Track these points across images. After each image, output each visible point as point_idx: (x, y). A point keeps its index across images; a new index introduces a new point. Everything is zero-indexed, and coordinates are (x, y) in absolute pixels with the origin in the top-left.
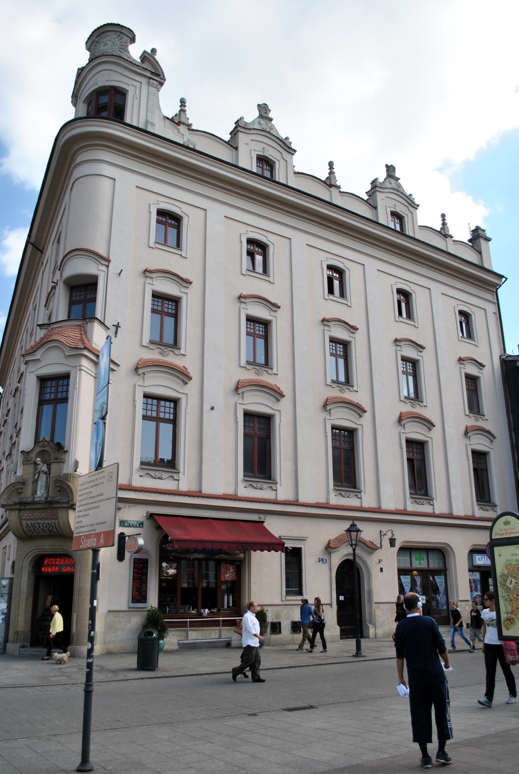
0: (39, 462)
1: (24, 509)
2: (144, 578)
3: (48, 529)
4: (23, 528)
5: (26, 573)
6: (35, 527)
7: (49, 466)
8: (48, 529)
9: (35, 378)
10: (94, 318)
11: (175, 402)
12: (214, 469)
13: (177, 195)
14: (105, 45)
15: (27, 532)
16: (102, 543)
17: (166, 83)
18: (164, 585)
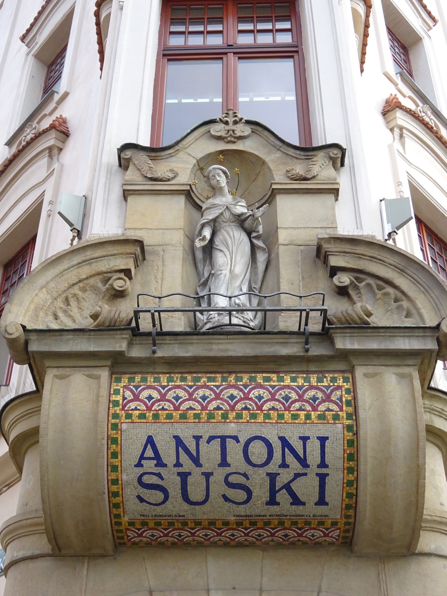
3: (273, 477)
6: (196, 461)
8: (273, 477)
15: (130, 492)
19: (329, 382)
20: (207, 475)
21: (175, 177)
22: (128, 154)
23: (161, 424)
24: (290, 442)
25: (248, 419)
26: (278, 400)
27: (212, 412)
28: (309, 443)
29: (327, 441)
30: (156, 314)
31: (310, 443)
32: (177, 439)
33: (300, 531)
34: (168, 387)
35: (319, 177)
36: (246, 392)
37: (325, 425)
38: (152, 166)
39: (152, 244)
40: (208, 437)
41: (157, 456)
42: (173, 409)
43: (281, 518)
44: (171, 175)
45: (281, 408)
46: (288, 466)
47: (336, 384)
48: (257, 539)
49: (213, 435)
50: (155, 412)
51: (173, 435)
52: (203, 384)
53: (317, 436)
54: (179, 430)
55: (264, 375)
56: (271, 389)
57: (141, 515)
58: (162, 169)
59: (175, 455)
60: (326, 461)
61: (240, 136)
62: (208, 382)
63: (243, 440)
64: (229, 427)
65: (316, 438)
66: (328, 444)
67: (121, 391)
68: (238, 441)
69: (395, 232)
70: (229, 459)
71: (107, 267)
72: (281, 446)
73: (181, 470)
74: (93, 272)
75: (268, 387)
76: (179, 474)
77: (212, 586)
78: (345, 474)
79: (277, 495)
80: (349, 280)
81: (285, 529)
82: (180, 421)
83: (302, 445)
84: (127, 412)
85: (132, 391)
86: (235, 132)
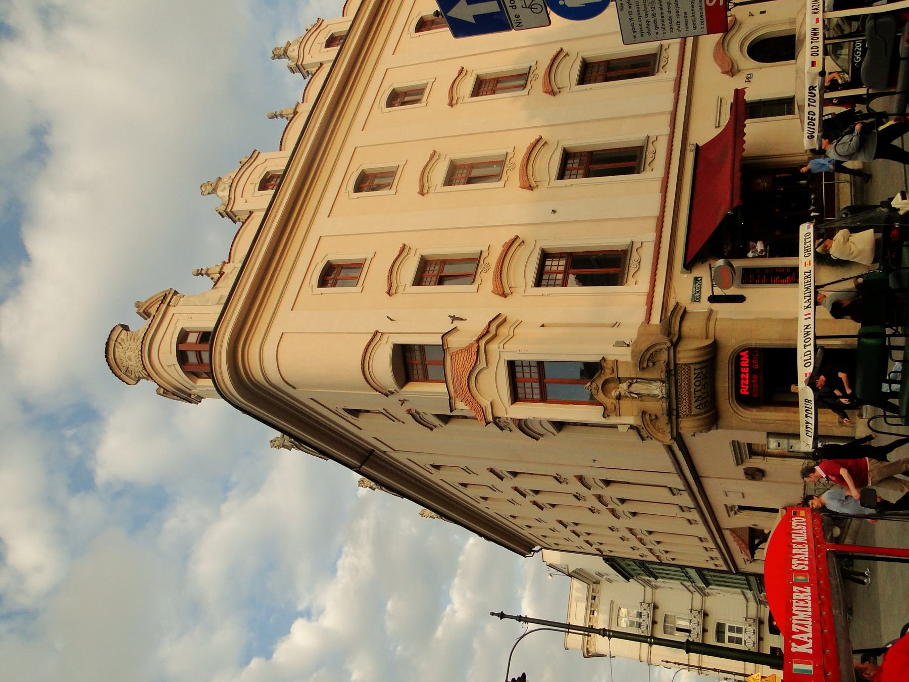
0: (617, 393)
1: (677, 409)
2: (767, 271)
4: (699, 415)
5: (760, 413)
7: (620, 380)
9: (514, 406)
10: (443, 348)
11: (545, 255)
12: (629, 212)
13: (340, 170)
14: (130, 358)
17: (175, 289)
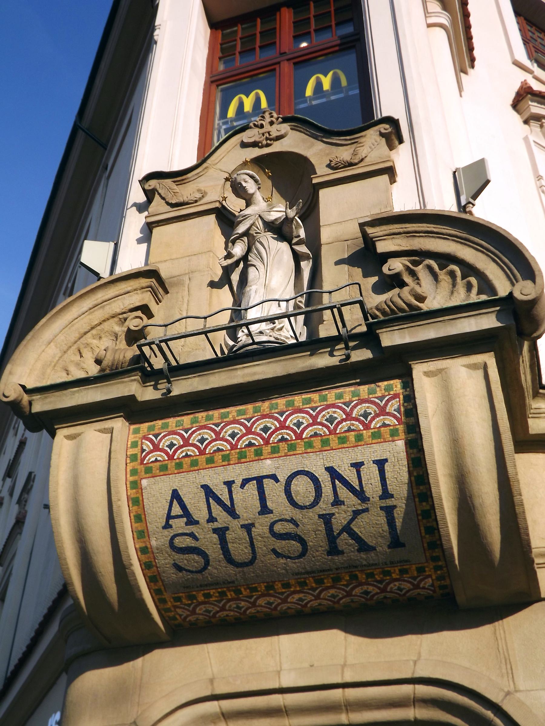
3: (327, 519)
6: (231, 511)
8: (327, 519)
16: (240, 604)
18: (266, 230)
19: (383, 392)
20: (248, 528)
21: (203, 196)
22: (153, 183)
23: (185, 473)
24: (340, 472)
25: (286, 451)
26: (321, 424)
27: (244, 450)
28: (364, 470)
29: (387, 464)
30: (163, 345)
31: (365, 470)
32: (206, 488)
33: (381, 584)
34: (192, 430)
35: (367, 161)
36: (282, 420)
37: (381, 444)
38: (178, 191)
39: (177, 274)
40: (241, 480)
41: (186, 513)
42: (198, 454)
43: (350, 570)
44: (198, 195)
45: (324, 432)
46: (343, 503)
47: (392, 393)
48: (334, 602)
49: (247, 477)
50: (177, 461)
51: (201, 484)
52: (232, 419)
53: (373, 459)
54: (207, 478)
55: (303, 397)
56: (311, 412)
57: (184, 587)
58: (186, 192)
59: (206, 509)
60: (389, 490)
61: (277, 136)
62: (237, 416)
63: (282, 477)
64: (264, 465)
65: (372, 462)
66: (388, 468)
67: (140, 443)
68: (277, 480)
69: (470, 203)
70: (269, 504)
71: (122, 307)
72: (330, 479)
73: (216, 525)
74: (107, 316)
75: (309, 410)
76: (215, 531)
77: (285, 666)
78: (417, 503)
79: (338, 541)
80: (401, 265)
81: (361, 584)
82: (207, 466)
83: (356, 473)
84: (147, 465)
85: (151, 441)
86: (271, 133)
